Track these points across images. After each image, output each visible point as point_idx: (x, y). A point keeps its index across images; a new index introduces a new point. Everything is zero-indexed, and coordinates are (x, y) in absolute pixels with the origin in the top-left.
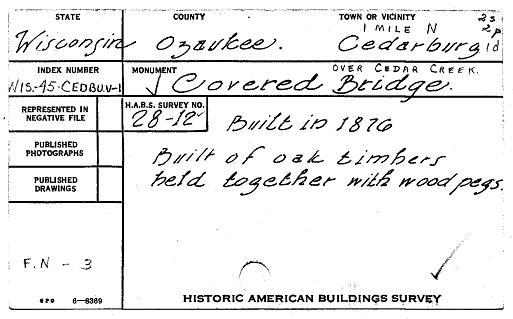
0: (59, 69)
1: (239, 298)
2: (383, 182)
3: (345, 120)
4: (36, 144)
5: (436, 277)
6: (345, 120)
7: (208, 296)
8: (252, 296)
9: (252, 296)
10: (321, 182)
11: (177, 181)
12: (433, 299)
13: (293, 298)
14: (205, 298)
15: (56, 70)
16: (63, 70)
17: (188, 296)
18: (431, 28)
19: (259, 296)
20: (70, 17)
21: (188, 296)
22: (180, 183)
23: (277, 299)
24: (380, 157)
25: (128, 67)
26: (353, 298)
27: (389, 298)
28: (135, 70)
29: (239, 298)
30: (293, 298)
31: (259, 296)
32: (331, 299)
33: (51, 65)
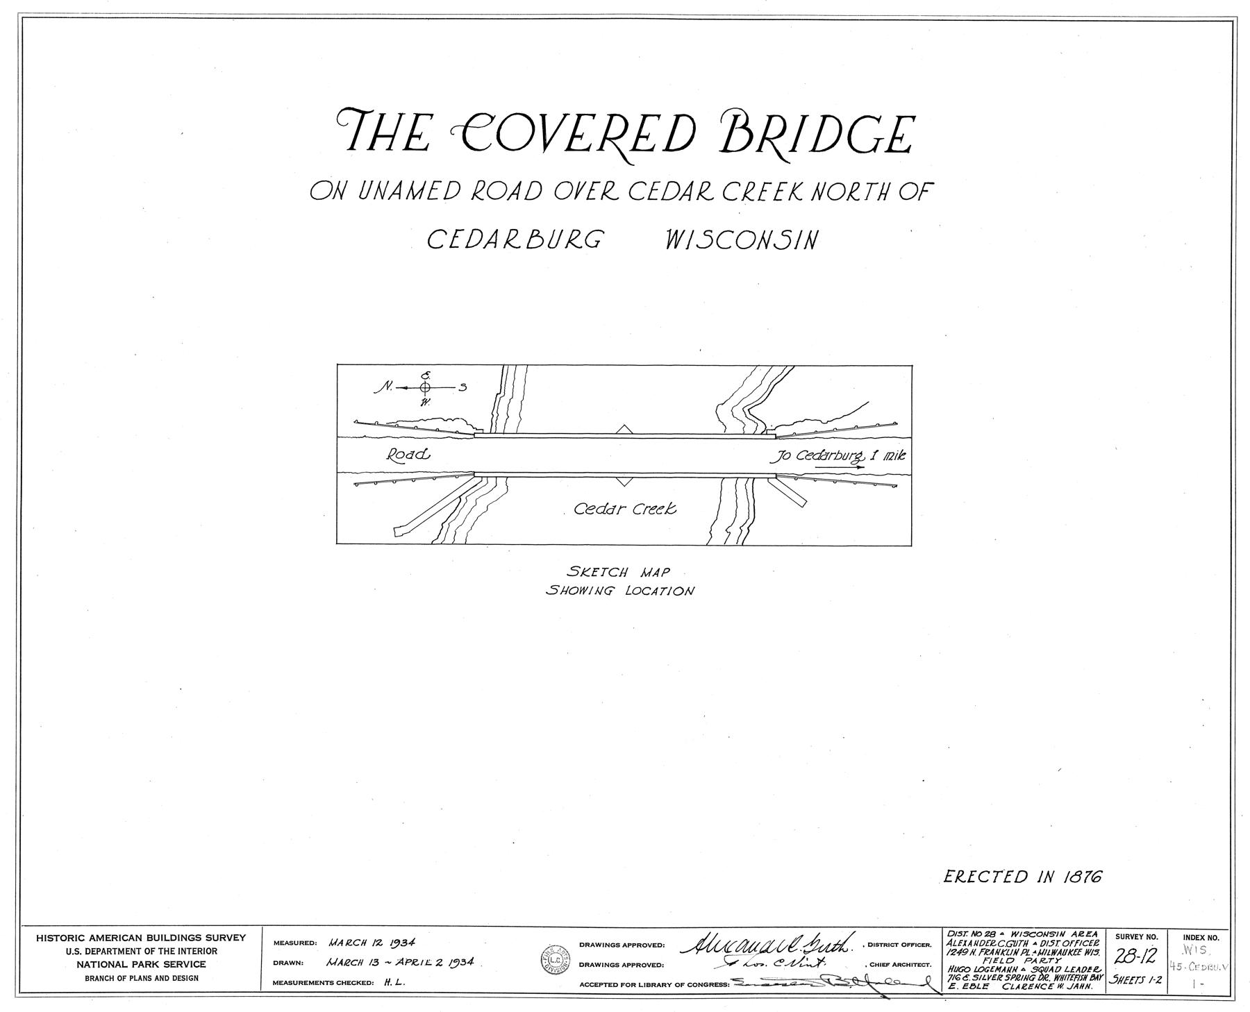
0: (1202, 938)
1: (81, 938)
3: (875, 453)
4: (1088, 986)
5: (432, 115)
6: (875, 453)
7: (57, 936)
8: (92, 936)
9: (92, 936)
10: (783, 964)
12: (239, 938)
13: (125, 938)
14: (54, 938)
15: (1200, 938)
17: (40, 936)
18: (1045, 978)
19: (97, 936)
21: (40, 936)
24: (832, 950)
27: (204, 938)
29: (81, 938)
30: (125, 938)
31: (97, 936)
32: (157, 938)
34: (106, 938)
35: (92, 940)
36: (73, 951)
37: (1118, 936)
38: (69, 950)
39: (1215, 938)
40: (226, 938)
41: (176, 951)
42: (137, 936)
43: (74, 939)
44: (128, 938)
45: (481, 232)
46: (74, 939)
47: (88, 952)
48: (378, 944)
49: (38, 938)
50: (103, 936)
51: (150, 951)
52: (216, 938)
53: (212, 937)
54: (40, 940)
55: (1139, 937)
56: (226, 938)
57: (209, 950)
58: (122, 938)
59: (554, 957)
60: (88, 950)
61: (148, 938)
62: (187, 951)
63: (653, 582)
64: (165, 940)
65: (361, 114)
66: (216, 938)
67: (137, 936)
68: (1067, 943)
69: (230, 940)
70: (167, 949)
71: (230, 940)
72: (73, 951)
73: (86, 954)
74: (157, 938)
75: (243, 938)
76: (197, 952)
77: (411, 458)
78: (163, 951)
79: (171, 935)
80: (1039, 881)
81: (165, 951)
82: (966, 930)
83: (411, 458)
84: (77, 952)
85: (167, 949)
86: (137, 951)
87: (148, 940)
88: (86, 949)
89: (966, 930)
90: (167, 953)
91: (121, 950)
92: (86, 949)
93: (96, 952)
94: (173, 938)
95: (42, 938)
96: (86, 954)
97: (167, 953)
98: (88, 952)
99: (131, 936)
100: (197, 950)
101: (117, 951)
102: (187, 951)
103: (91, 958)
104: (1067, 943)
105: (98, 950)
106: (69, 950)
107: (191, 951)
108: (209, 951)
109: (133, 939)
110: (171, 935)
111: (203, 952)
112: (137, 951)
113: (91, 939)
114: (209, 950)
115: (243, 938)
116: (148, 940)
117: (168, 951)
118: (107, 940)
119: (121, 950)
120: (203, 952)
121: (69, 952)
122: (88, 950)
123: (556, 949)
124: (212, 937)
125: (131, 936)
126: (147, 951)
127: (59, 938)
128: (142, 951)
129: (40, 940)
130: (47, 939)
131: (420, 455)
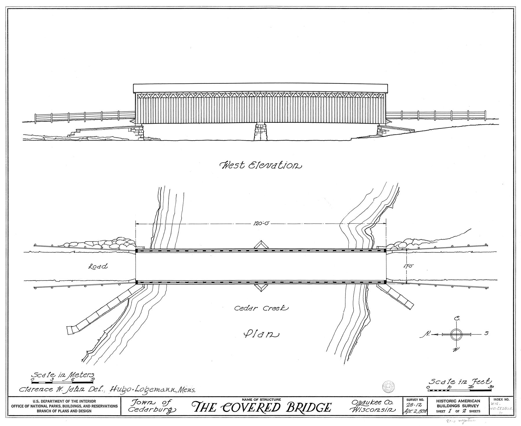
1: (455, 401)
8: (459, 400)
9: (459, 400)
12: (476, 406)
13: (473, 401)
14: (444, 401)
29: (455, 401)
30: (473, 401)
31: (462, 400)
32: (441, 406)
34: (465, 401)
36: (36, 401)
37: (407, 400)
38: (34, 401)
39: (422, 400)
41: (79, 401)
42: (478, 400)
43: (470, 401)
44: (474, 401)
46: (470, 401)
47: (42, 402)
49: (437, 401)
53: (465, 405)
54: (438, 402)
55: (416, 400)
56: (471, 406)
57: (112, 406)
61: (438, 406)
62: (83, 401)
64: (445, 407)
66: (466, 406)
67: (478, 400)
68: (373, 410)
69: (472, 407)
70: (75, 401)
71: (472, 407)
72: (36, 401)
74: (441, 406)
75: (478, 406)
76: (87, 402)
77: (100, 268)
78: (73, 401)
80: (254, 225)
83: (100, 268)
84: (38, 401)
85: (75, 401)
86: (62, 401)
87: (438, 407)
88: (79, 410)
90: (75, 402)
93: (45, 402)
95: (439, 401)
97: (75, 402)
98: (42, 402)
99: (476, 400)
100: (87, 401)
101: (54, 401)
102: (83, 401)
104: (373, 410)
105: (46, 401)
106: (34, 401)
107: (85, 401)
108: (92, 401)
109: (476, 401)
111: (90, 402)
112: (62, 401)
113: (459, 401)
114: (112, 406)
115: (478, 406)
116: (438, 407)
118: (465, 402)
120: (90, 402)
122: (80, 411)
125: (476, 400)
126: (67, 401)
127: (446, 401)
128: (64, 401)
130: (441, 401)
131: (104, 267)
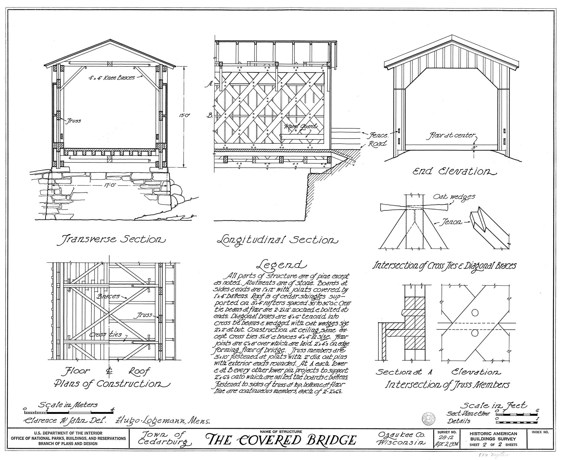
1: (490, 434)
2: (120, 419)
7: (479, 433)
11: (128, 384)
12: (513, 439)
13: (510, 434)
14: (478, 434)
15: (539, 432)
16: (542, 432)
17: (471, 433)
19: (497, 433)
20: (37, 438)
21: (471, 433)
22: (127, 383)
23: (504, 434)
25: (436, 431)
26: (483, 439)
28: (533, 432)
29: (490, 434)
30: (510, 434)
31: (497, 433)
32: (475, 439)
33: (537, 430)
35: (495, 435)
36: (37, 433)
40: (507, 439)
41: (84, 433)
42: (515, 433)
44: (511, 434)
45: (206, 435)
47: (44, 433)
48: (69, 406)
49: (470, 434)
50: (500, 433)
51: (293, 330)
52: (502, 439)
53: (501, 439)
54: (471, 434)
56: (507, 439)
58: (508, 434)
59: (428, 417)
60: (85, 443)
61: (471, 439)
62: (89, 433)
63: (275, 430)
64: (479, 440)
65: (213, 435)
66: (502, 439)
67: (515, 433)
69: (509, 440)
70: (79, 432)
71: (509, 440)
72: (37, 433)
73: (43, 434)
74: (475, 439)
76: (93, 434)
78: (78, 433)
79: (482, 438)
81: (79, 433)
82: (229, 432)
84: (39, 433)
85: (79, 432)
88: (84, 442)
89: (229, 432)
90: (79, 434)
91: (59, 432)
92: (84, 442)
93: (47, 433)
94: (483, 439)
95: (472, 434)
96: (43, 434)
97: (79, 434)
98: (44, 433)
99: (512, 433)
101: (57, 433)
102: (89, 433)
103: (90, 441)
105: (49, 433)
107: (90, 433)
108: (98, 433)
109: (495, 434)
110: (482, 438)
111: (96, 433)
112: (66, 433)
117: (80, 433)
119: (59, 432)
120: (96, 433)
121: (35, 433)
122: (85, 443)
123: (429, 414)
124: (91, 443)
125: (512, 433)
126: (71, 433)
127: (480, 434)
128: (68, 433)
129: (471, 434)
130: (475, 434)
